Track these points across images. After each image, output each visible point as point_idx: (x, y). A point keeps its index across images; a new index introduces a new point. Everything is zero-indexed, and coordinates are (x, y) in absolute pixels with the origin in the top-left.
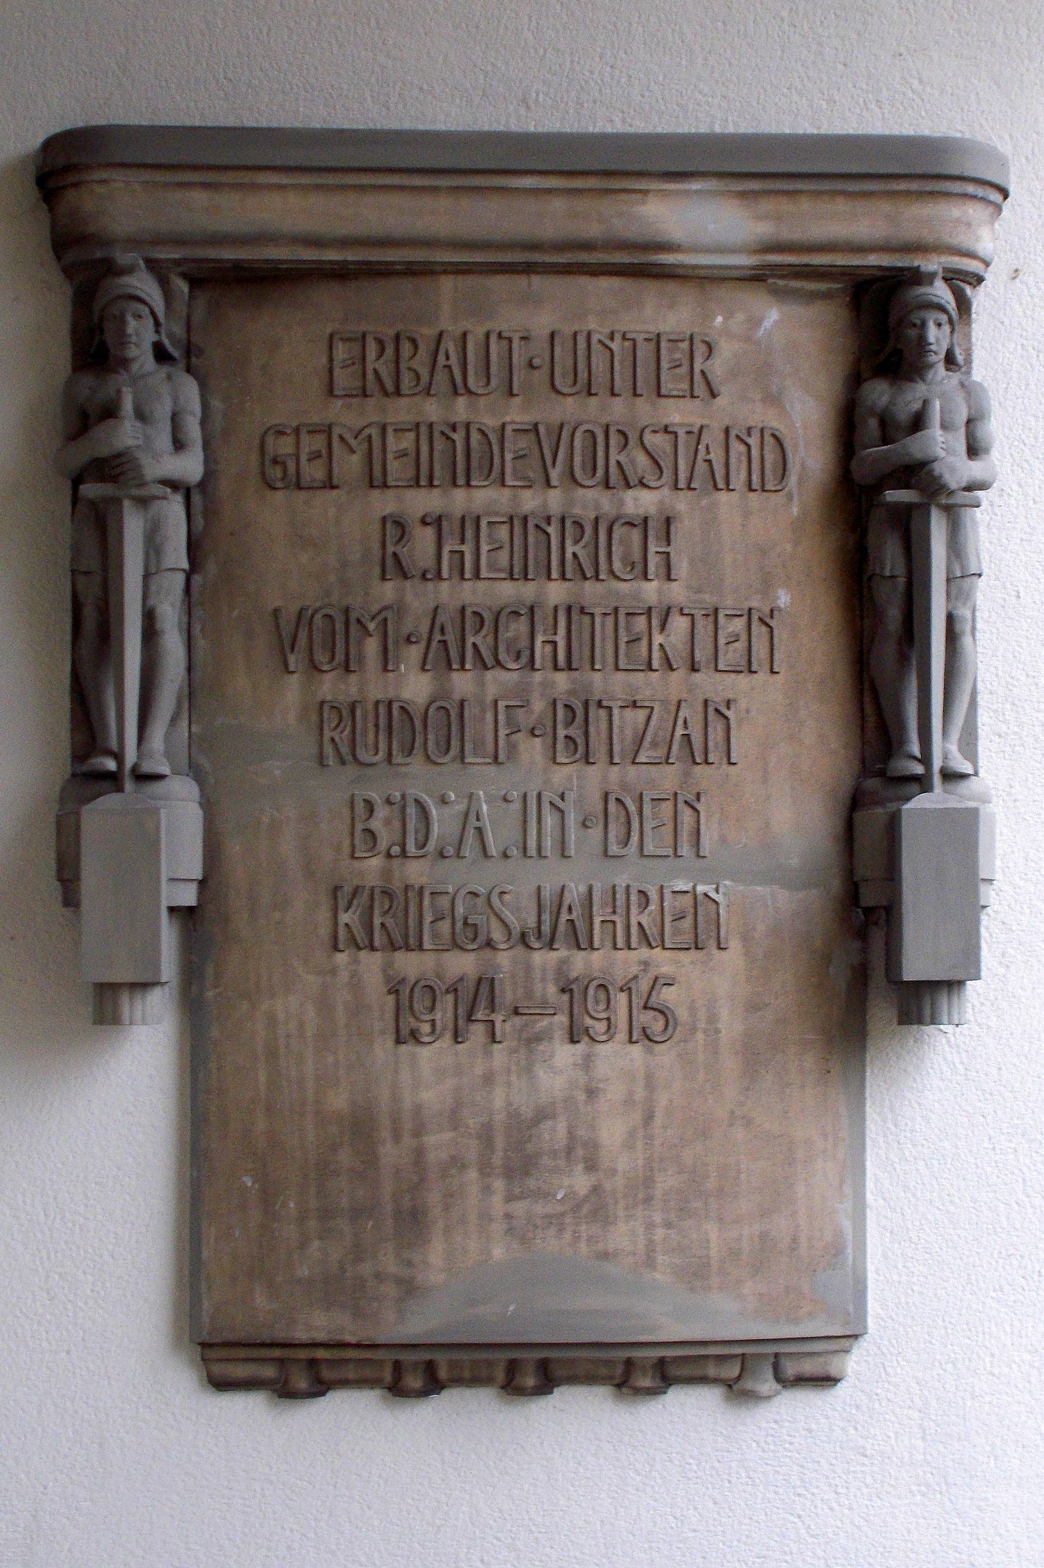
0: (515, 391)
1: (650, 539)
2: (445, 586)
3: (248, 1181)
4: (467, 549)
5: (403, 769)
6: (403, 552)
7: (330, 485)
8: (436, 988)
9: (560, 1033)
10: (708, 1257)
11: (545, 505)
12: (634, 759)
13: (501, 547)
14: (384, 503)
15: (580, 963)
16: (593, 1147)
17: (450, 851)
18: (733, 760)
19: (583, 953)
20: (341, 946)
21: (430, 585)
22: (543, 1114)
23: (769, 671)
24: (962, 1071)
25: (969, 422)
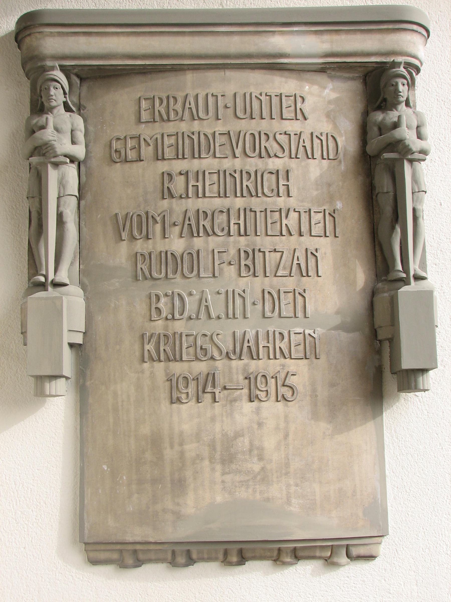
0: (219, 118)
1: (280, 179)
2: (190, 200)
3: (105, 467)
4: (200, 184)
5: (173, 281)
6: (172, 187)
7: (140, 160)
8: (189, 378)
9: (245, 397)
10: (315, 499)
11: (233, 165)
12: (276, 274)
13: (214, 183)
14: (163, 167)
15: (254, 366)
16: (261, 449)
17: (194, 316)
18: (319, 275)
19: (254, 361)
20: (146, 360)
21: (183, 200)
22: (238, 435)
23: (334, 236)
24: (426, 413)
25: (418, 127)
